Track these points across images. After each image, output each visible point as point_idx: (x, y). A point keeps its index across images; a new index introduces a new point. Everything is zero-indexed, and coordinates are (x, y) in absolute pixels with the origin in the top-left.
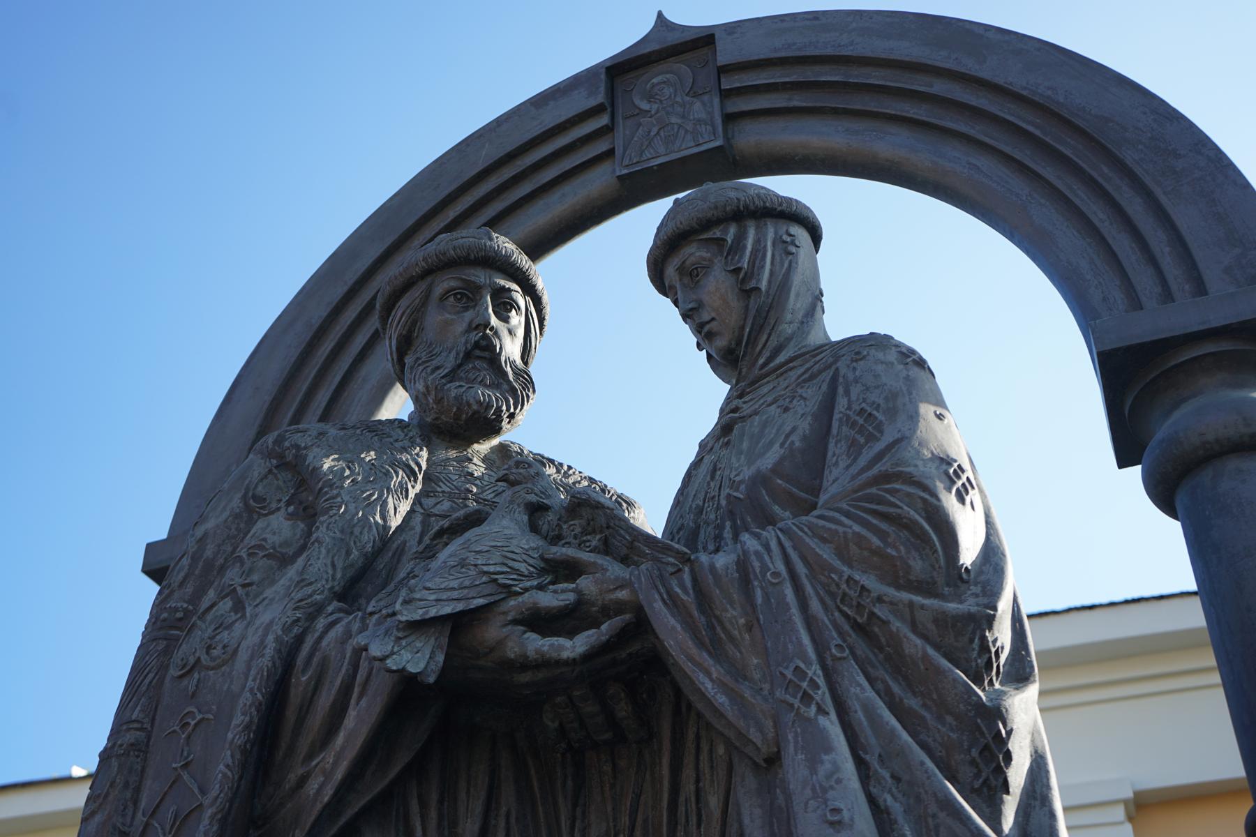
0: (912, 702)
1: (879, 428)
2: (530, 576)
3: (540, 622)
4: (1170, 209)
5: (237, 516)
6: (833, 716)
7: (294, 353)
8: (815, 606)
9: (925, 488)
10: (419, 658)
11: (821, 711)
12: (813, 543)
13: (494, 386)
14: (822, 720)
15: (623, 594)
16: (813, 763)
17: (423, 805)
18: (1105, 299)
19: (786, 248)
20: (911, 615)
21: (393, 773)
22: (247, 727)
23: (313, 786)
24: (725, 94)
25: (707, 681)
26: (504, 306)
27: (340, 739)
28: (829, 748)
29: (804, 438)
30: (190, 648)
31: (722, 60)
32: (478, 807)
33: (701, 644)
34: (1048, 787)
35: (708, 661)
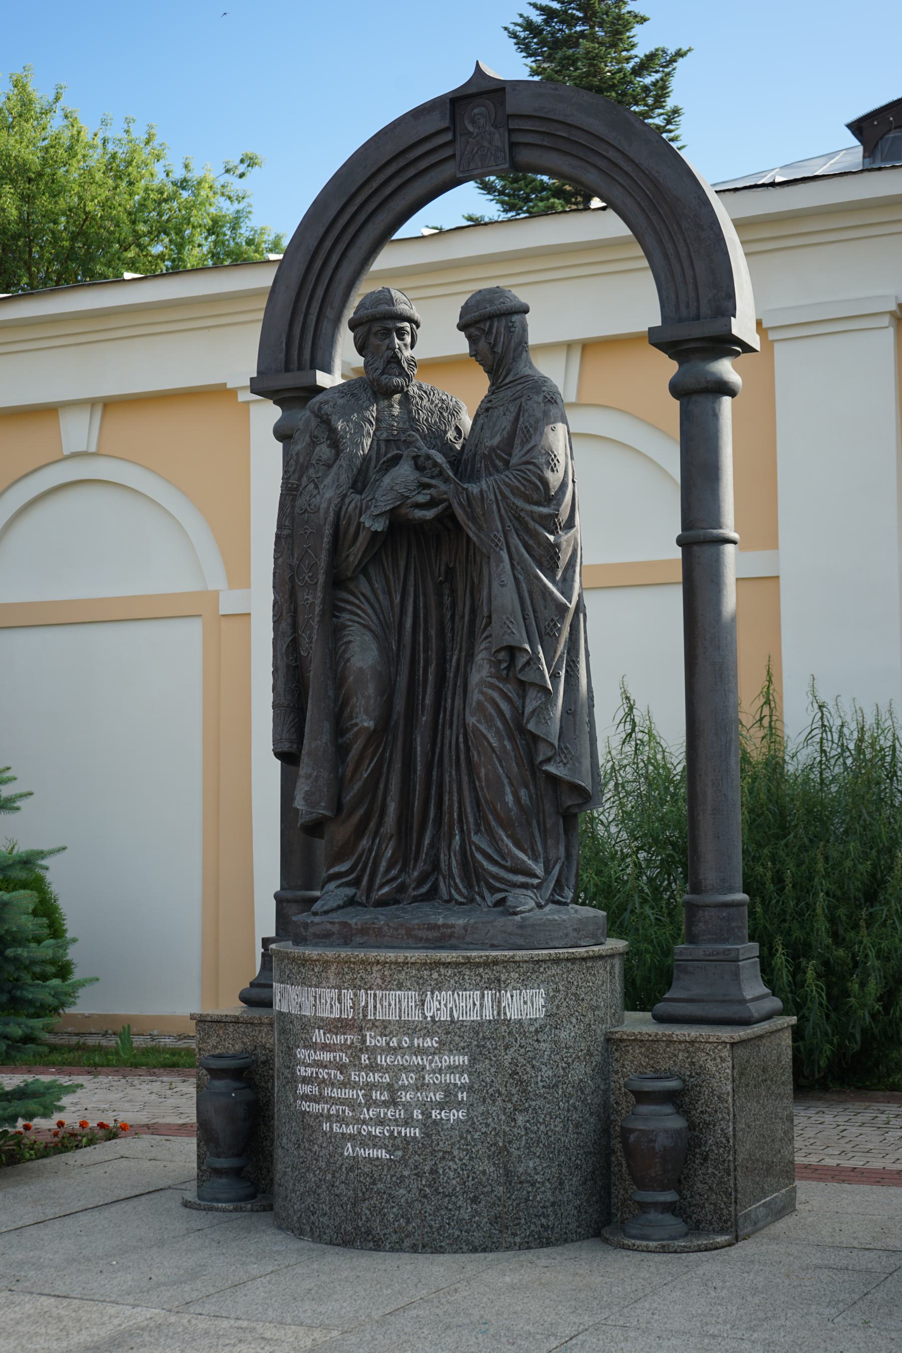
0: (531, 542)
1: (530, 437)
2: (415, 490)
3: (419, 506)
4: (694, 261)
5: (309, 445)
6: (505, 550)
7: (303, 267)
8: (503, 511)
9: (540, 469)
10: (379, 526)
11: (501, 549)
12: (502, 487)
13: (400, 375)
14: (501, 552)
15: (445, 496)
16: (498, 566)
17: (387, 557)
18: (668, 297)
19: (509, 329)
20: (531, 514)
21: (376, 549)
22: (329, 543)
23: (351, 558)
24: (511, 131)
25: (471, 530)
26: (401, 334)
27: (358, 544)
28: (502, 561)
29: (508, 433)
30: (301, 502)
31: (510, 110)
32: (404, 555)
33: (469, 519)
34: (576, 561)
35: (470, 524)
